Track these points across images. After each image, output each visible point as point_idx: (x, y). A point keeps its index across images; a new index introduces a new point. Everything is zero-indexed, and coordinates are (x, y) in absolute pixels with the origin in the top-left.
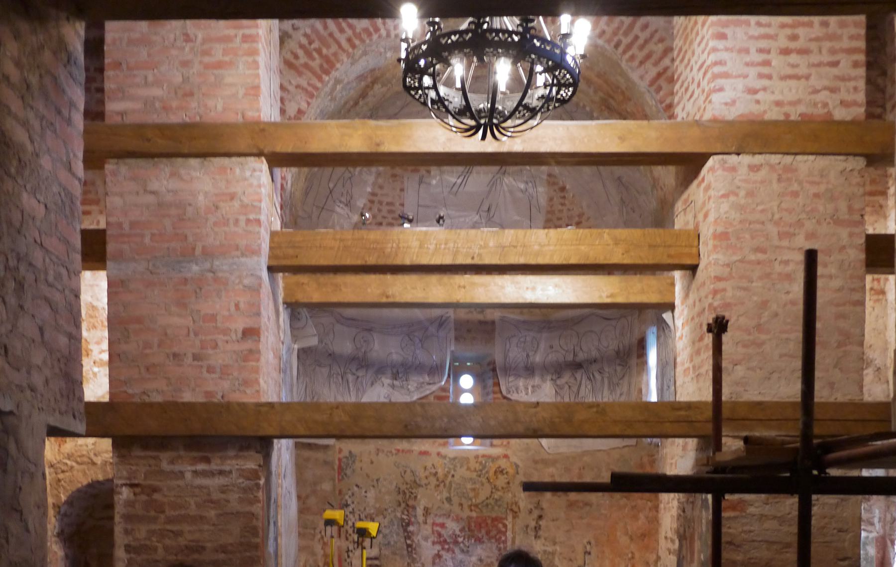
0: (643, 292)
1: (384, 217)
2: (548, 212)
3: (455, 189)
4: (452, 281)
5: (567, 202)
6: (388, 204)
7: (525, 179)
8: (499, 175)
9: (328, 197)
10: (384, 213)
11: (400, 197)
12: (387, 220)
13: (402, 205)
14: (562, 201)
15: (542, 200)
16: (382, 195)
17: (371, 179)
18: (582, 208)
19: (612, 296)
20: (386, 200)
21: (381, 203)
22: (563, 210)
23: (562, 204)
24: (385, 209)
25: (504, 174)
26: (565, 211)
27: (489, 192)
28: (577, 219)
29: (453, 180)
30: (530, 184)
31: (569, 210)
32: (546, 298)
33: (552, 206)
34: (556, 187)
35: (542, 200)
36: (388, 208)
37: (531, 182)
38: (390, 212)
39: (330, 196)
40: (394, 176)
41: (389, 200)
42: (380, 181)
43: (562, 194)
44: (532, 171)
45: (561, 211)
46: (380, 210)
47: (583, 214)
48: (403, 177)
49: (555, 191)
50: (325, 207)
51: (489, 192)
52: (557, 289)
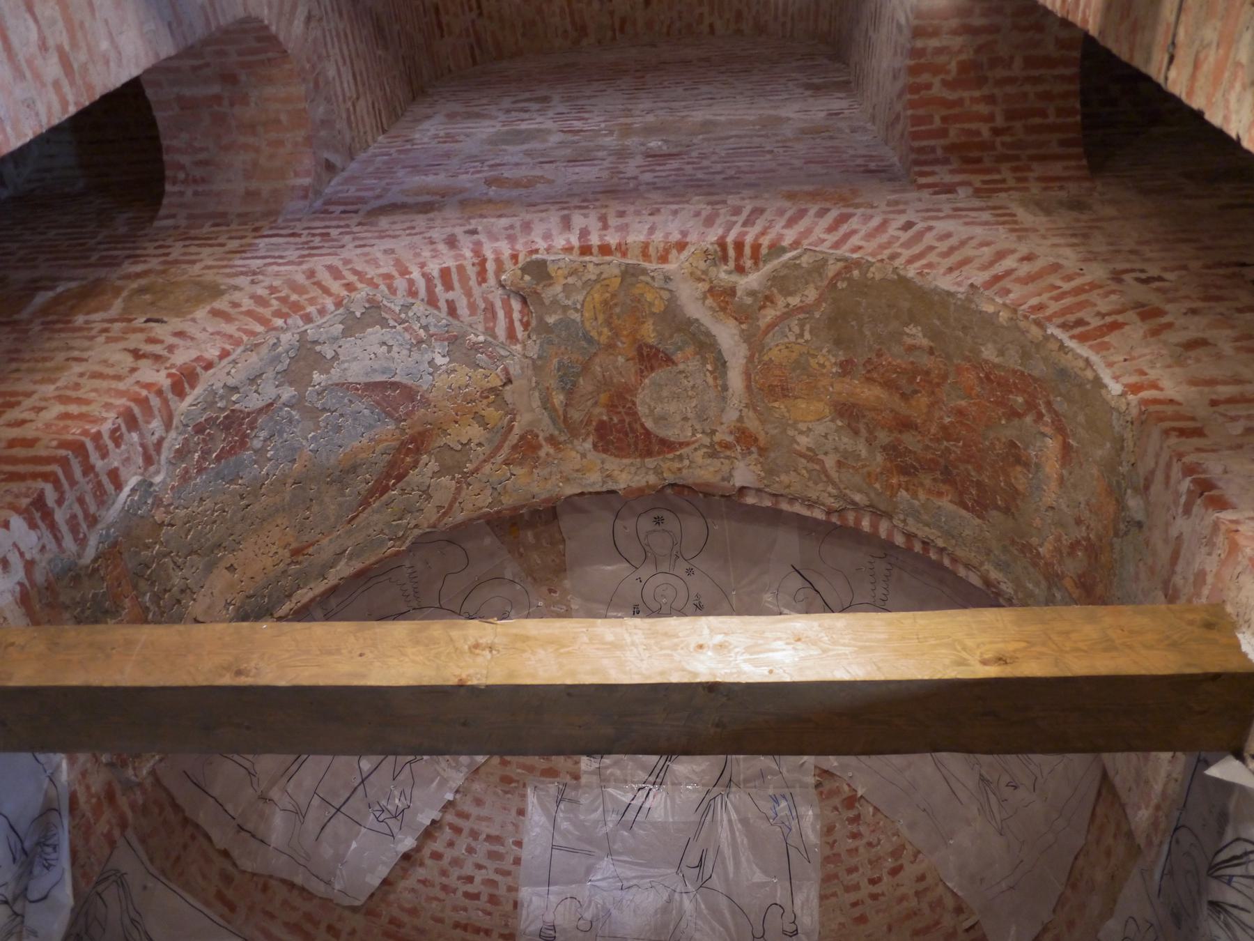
0: (1109, 646)
1: (479, 867)
2: (827, 860)
3: (630, 816)
4: (455, 633)
5: (863, 829)
6: (489, 838)
7: (771, 792)
8: (716, 790)
9: (355, 789)
10: (480, 857)
11: (516, 826)
12: (483, 871)
13: (519, 844)
14: (853, 828)
15: (810, 832)
16: (480, 818)
17: (457, 778)
18: (897, 834)
19: (1001, 660)
20: (485, 829)
21: (474, 834)
22: (856, 850)
23: (855, 836)
24: (483, 847)
25: (729, 786)
26: (861, 850)
27: (701, 824)
28: (890, 863)
29: (626, 799)
30: (783, 804)
31: (870, 844)
32: (765, 671)
33: (832, 845)
34: (837, 801)
35: (810, 832)
36: (487, 846)
37: (784, 797)
38: (492, 855)
39: (360, 790)
40: (506, 780)
41: (494, 831)
42: (477, 787)
43: (851, 814)
44: (784, 770)
45: (853, 852)
46: (470, 850)
47: (903, 847)
48: (524, 786)
49: (836, 809)
50: (342, 810)
51: (701, 824)
52: (800, 645)
